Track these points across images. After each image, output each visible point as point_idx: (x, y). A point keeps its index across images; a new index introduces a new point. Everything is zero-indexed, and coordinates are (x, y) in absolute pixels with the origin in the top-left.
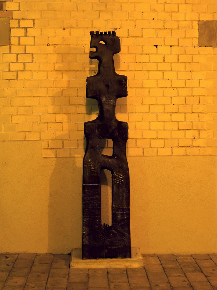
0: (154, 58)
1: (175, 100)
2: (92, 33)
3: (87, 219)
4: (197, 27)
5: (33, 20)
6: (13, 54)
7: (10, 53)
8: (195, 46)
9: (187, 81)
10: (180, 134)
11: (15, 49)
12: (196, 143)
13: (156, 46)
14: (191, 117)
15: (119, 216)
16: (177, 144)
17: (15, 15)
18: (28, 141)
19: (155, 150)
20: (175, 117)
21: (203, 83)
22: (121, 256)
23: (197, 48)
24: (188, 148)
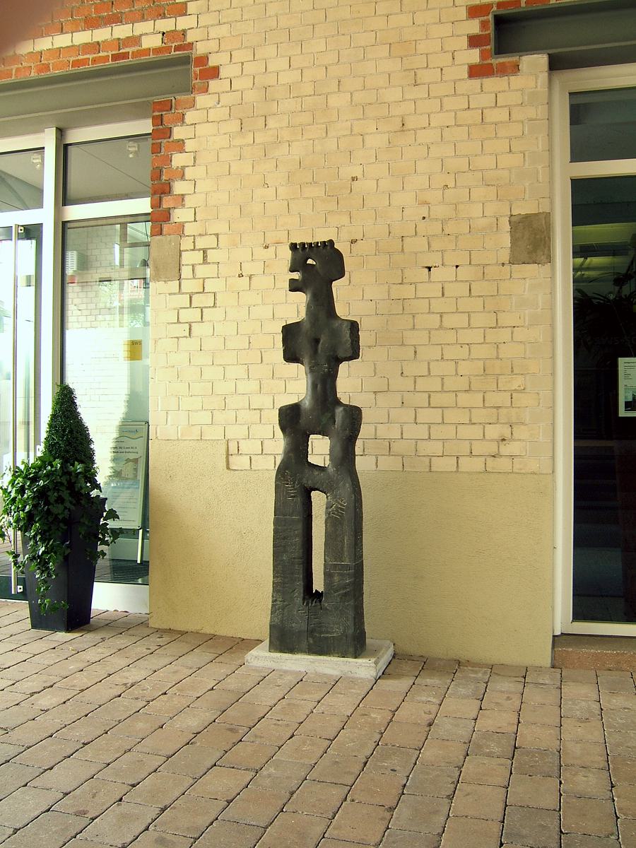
0: (424, 290)
1: (464, 368)
2: (293, 247)
3: (279, 580)
4: (508, 228)
5: (217, 235)
6: (183, 294)
7: (180, 292)
8: (503, 264)
9: (488, 330)
10: (475, 432)
11: (188, 286)
12: (506, 449)
13: (429, 268)
14: (493, 399)
15: (335, 578)
16: (469, 451)
17: (189, 229)
18: (206, 440)
19: (427, 460)
20: (464, 399)
21: (520, 335)
22: (338, 653)
23: (507, 267)
24: (490, 460)
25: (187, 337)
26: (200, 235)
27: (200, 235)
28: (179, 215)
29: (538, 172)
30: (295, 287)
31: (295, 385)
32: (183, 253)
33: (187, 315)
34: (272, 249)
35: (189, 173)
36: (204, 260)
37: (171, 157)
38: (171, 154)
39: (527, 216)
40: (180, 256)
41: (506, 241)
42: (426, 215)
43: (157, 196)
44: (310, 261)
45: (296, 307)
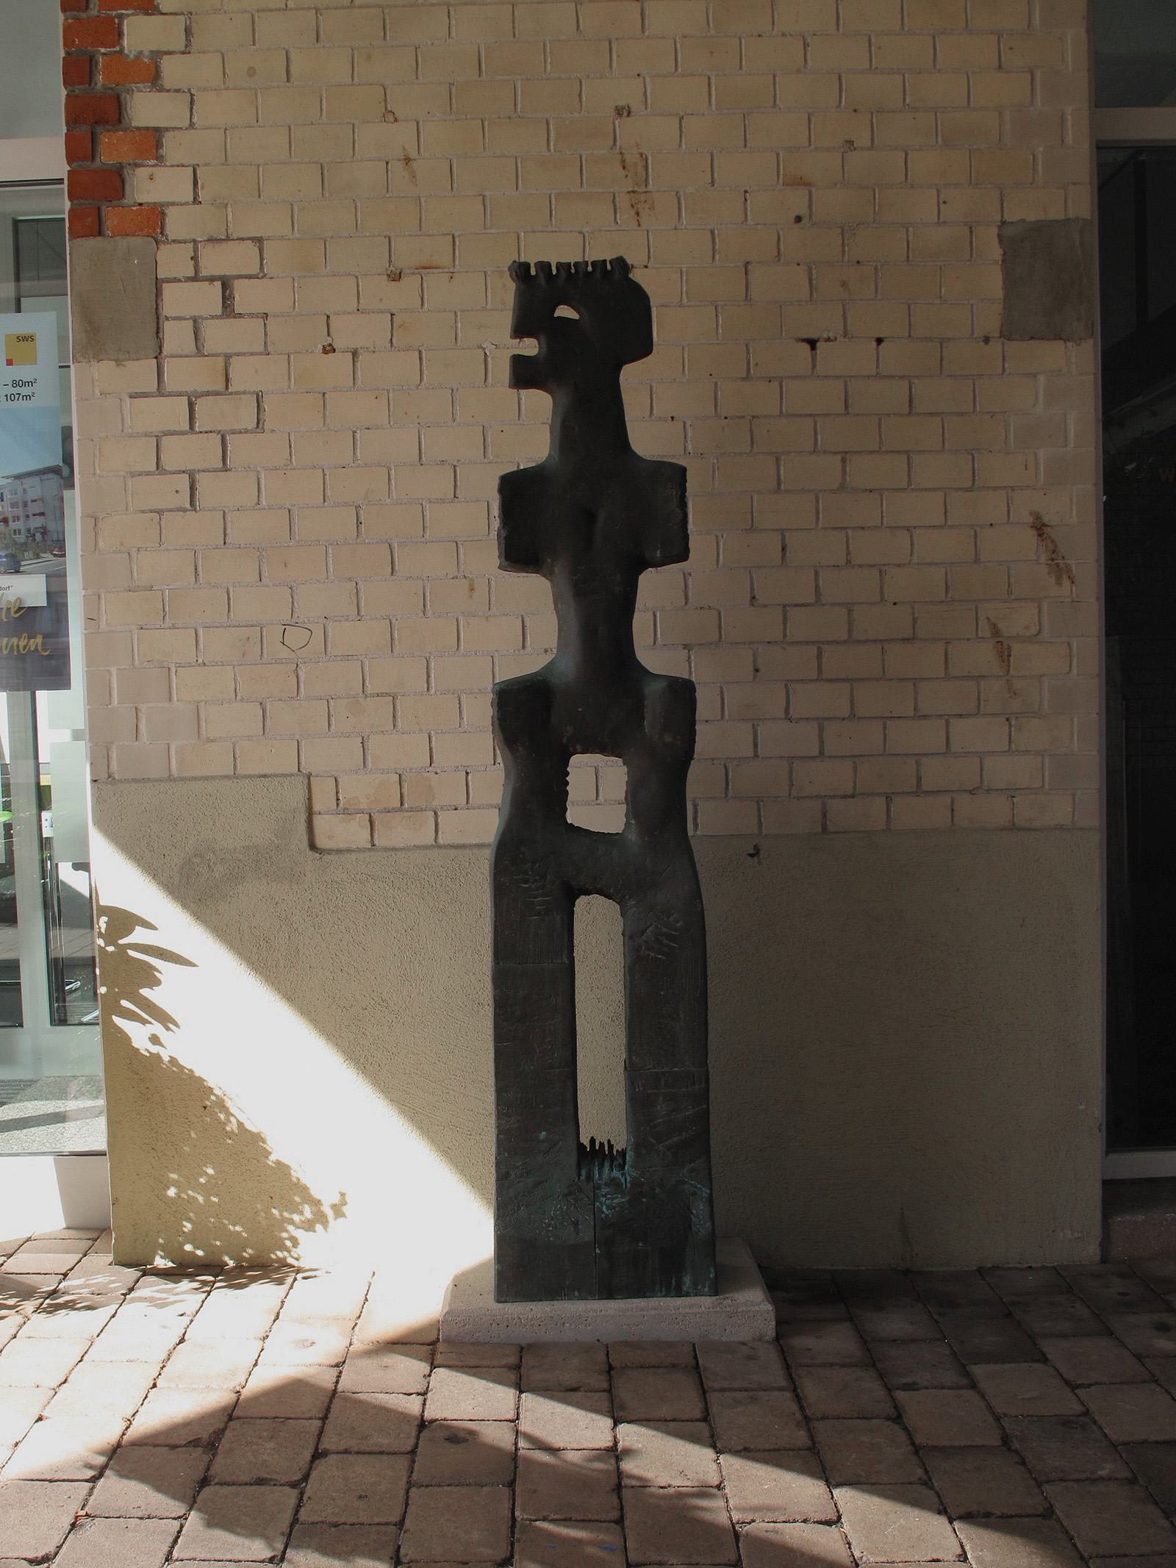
2: (521, 272)
4: (996, 252)
7: (161, 391)
8: (987, 340)
11: (181, 374)
13: (812, 343)
17: (176, 224)
25: (185, 510)
26: (212, 240)
27: (212, 240)
28: (148, 186)
29: (1063, 121)
30: (524, 374)
31: (526, 625)
32: (167, 288)
33: (180, 453)
34: (410, 283)
35: (172, 70)
36: (225, 306)
37: (121, 24)
38: (121, 17)
39: (1039, 227)
40: (158, 293)
41: (993, 282)
42: (803, 211)
43: (83, 130)
44: (564, 312)
45: (528, 431)
